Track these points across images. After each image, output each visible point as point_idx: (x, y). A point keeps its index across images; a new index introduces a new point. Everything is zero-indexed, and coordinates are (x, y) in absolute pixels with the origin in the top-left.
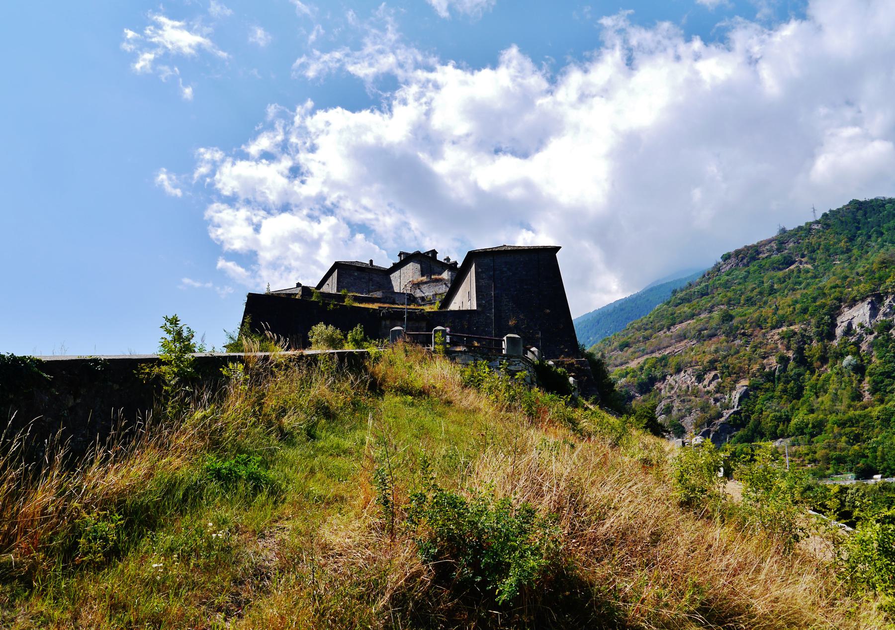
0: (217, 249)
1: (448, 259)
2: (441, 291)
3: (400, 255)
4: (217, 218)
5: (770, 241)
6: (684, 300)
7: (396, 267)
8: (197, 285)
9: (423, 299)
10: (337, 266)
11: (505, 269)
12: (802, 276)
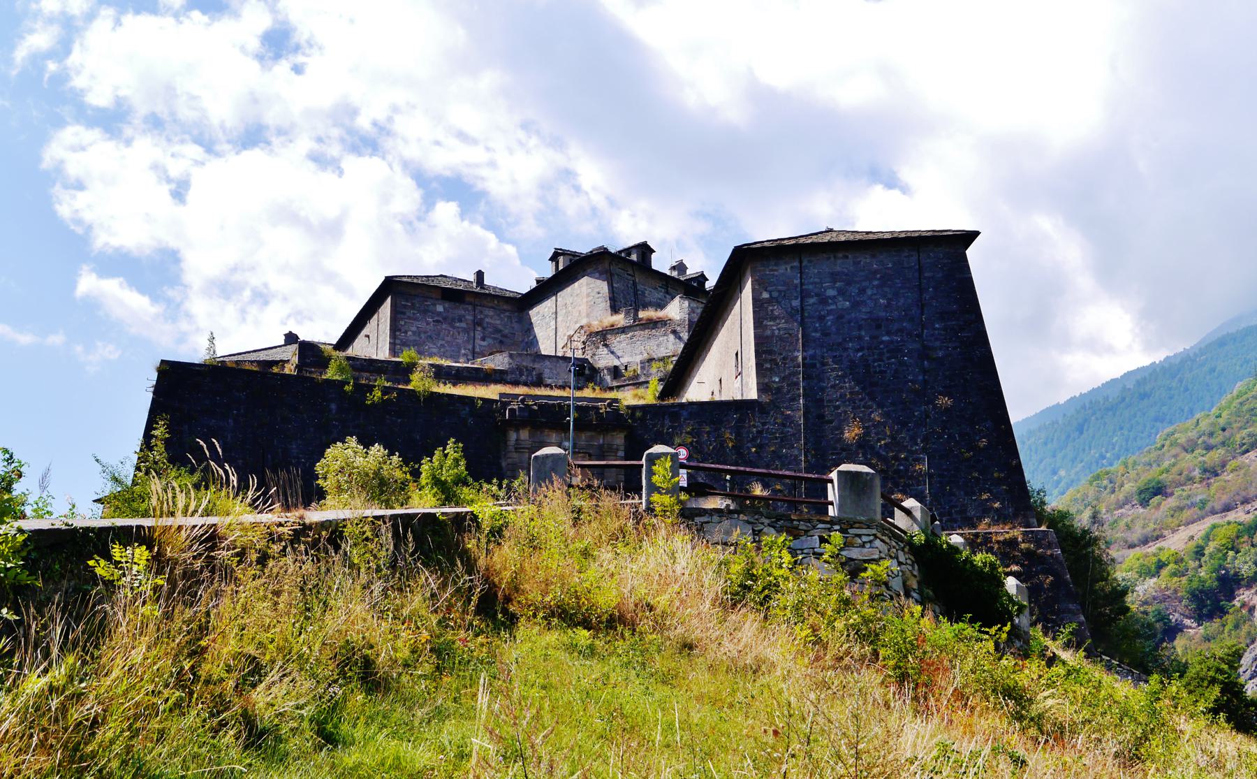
0: (74, 245)
1: (681, 267)
2: (662, 352)
3: (554, 258)
4: (74, 166)
7: (545, 289)
8: (25, 339)
9: (616, 372)
10: (391, 287)
11: (831, 293)
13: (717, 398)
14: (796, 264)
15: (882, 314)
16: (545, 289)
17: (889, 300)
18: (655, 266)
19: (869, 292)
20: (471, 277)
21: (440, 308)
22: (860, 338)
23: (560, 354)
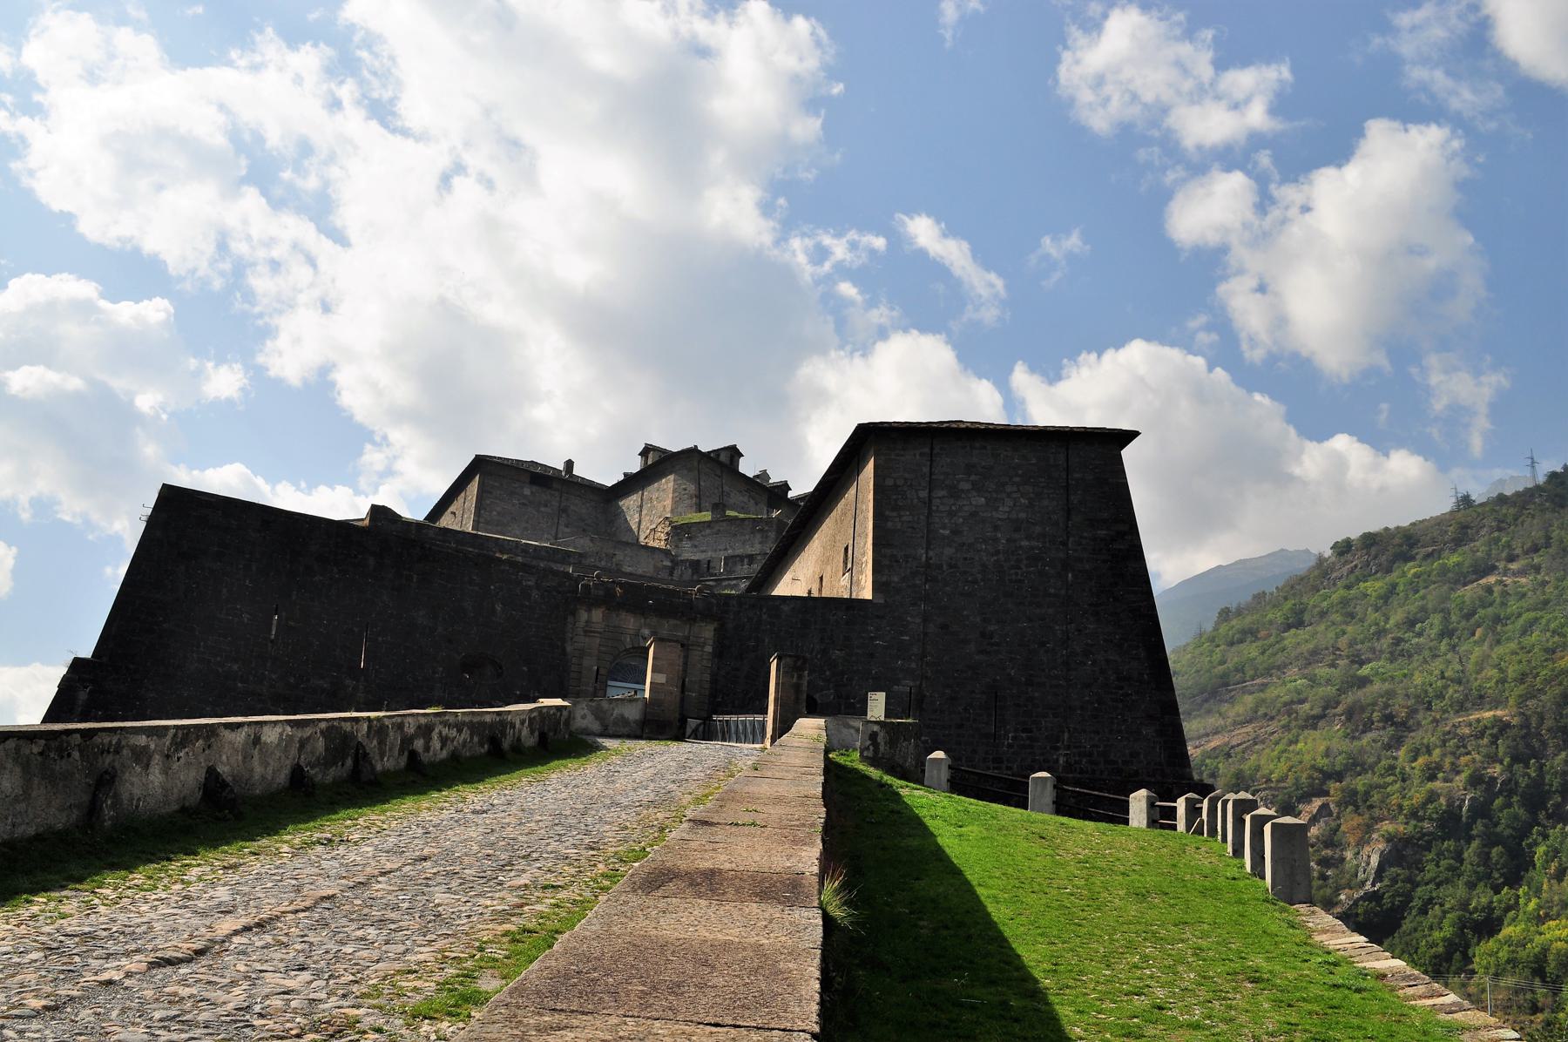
3: (647, 451)
5: (1439, 522)
6: (1249, 634)
12: (1513, 606)
13: (815, 594)
14: (927, 450)
15: (1023, 515)
18: (741, 470)
19: (1009, 489)
20: (561, 467)
21: (527, 492)
22: (996, 540)
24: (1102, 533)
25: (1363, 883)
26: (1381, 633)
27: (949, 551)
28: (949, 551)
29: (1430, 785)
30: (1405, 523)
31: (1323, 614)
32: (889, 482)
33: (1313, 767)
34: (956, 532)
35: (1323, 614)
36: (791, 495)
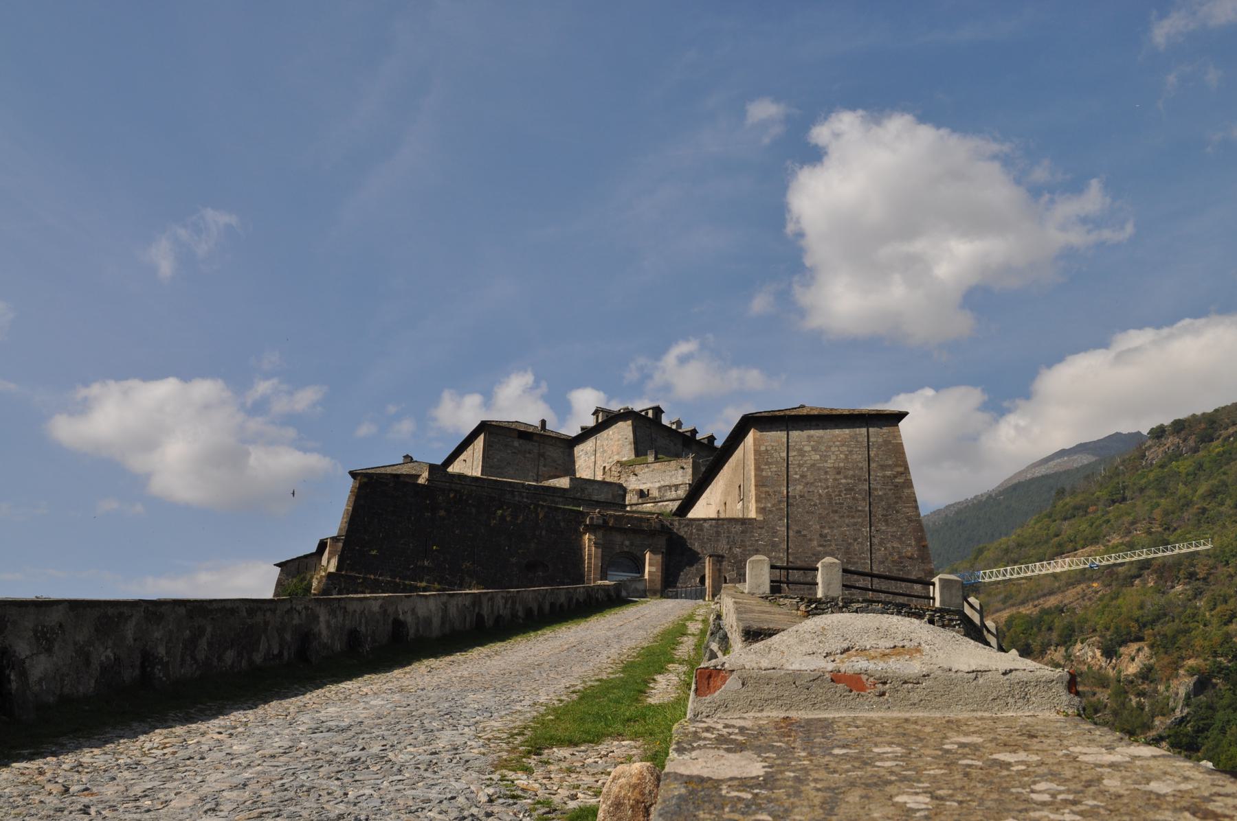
3: (596, 413)
7: (587, 433)
10: (484, 427)
13: (722, 516)
16: (587, 433)
17: (846, 456)
19: (833, 449)
20: (537, 423)
21: (516, 444)
22: (827, 480)
23: (599, 478)
24: (888, 473)
25: (1173, 710)
26: (1189, 504)
27: (799, 487)
28: (799, 487)
29: (1225, 628)
30: (1210, 410)
31: (1142, 490)
32: (763, 448)
33: (1131, 618)
34: (803, 476)
35: (1142, 490)
36: (698, 437)
